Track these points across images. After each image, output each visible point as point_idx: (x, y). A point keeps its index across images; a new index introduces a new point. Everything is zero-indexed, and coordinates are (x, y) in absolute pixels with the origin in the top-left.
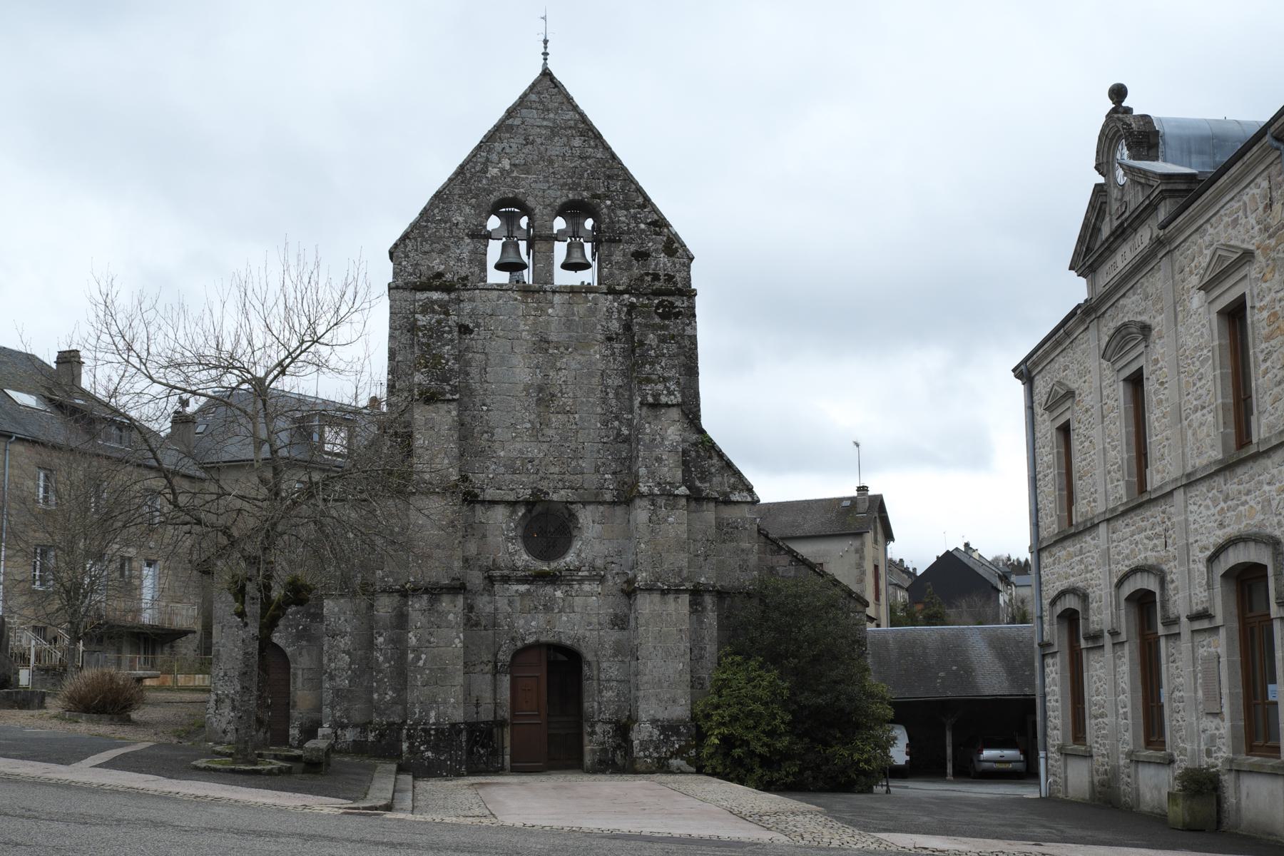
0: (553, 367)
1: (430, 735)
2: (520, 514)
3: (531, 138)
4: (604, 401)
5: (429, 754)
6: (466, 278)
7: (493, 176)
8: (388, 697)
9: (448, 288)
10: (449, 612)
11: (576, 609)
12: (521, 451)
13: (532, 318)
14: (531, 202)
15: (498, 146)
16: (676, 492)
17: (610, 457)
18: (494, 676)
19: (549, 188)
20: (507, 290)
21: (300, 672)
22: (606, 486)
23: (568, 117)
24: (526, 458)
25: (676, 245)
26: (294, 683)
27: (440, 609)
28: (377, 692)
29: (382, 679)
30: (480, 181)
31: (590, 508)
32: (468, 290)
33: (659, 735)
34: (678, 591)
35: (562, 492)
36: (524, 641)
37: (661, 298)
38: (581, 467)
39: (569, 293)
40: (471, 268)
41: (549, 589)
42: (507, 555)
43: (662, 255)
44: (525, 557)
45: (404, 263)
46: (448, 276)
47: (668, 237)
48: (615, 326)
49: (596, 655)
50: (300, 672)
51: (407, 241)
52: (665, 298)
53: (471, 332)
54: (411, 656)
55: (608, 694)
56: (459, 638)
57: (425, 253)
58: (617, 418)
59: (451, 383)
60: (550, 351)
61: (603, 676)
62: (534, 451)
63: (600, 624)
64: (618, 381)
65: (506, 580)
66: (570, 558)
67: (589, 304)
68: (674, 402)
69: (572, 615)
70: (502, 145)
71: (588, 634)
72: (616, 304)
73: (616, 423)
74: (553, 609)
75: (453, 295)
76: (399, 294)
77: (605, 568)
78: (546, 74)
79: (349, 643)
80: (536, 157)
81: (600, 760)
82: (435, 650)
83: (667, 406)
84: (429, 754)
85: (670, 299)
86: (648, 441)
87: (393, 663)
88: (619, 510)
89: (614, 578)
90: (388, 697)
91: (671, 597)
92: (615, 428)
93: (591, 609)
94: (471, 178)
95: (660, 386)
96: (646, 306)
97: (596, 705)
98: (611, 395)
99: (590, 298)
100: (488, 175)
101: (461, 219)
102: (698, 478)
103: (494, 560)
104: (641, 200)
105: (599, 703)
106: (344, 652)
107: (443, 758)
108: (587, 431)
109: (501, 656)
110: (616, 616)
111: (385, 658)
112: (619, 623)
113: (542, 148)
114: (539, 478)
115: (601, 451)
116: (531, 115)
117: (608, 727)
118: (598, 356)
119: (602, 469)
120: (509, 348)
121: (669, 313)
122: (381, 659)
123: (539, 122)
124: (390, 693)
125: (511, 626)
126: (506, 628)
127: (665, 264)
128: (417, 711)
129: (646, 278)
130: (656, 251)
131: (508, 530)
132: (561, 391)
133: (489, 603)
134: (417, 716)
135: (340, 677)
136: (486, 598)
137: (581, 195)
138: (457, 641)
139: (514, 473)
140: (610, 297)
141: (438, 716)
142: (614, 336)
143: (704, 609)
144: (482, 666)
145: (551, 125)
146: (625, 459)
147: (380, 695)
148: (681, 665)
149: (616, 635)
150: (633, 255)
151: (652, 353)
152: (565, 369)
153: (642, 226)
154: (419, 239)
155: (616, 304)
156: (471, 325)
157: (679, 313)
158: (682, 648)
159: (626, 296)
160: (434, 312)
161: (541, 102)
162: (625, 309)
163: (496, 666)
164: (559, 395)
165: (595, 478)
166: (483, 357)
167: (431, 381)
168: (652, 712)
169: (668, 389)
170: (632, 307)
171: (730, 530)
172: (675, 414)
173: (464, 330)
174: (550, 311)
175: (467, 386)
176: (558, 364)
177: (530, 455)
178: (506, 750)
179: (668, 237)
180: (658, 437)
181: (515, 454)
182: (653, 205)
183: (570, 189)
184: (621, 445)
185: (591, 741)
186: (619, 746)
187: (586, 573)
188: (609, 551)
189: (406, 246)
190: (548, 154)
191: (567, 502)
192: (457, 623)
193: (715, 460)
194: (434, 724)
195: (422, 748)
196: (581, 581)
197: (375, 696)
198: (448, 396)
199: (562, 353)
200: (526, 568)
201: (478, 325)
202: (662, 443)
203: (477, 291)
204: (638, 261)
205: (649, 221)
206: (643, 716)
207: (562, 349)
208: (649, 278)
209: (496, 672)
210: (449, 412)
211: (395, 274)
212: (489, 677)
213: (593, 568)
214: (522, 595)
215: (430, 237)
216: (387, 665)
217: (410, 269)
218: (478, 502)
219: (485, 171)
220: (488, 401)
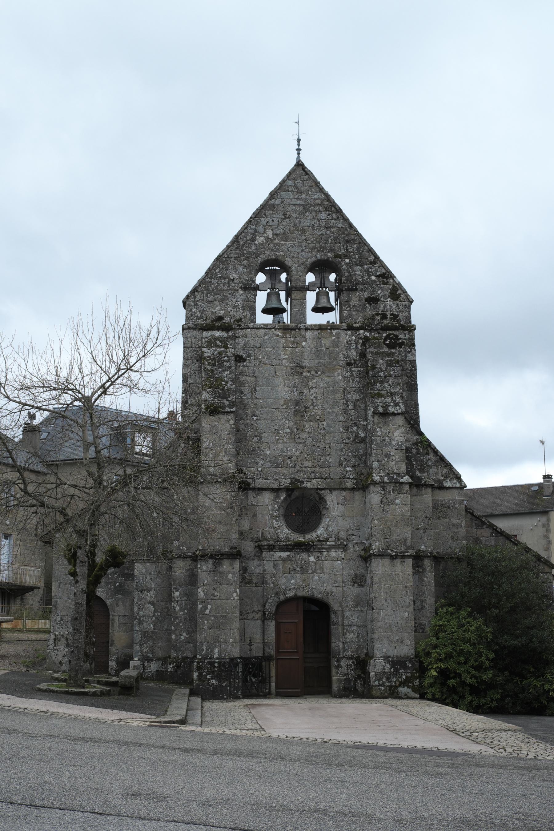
0: (306, 386)
1: (215, 667)
2: (282, 498)
3: (288, 213)
4: (346, 411)
5: (214, 681)
6: (240, 320)
7: (260, 243)
8: (182, 638)
9: (227, 328)
10: (229, 573)
11: (325, 570)
12: (282, 450)
13: (290, 349)
14: (288, 262)
15: (263, 220)
16: (402, 480)
17: (350, 454)
18: (263, 621)
19: (302, 251)
20: (271, 329)
21: (117, 618)
22: (347, 476)
23: (316, 197)
24: (286, 456)
25: (399, 292)
26: (113, 626)
27: (222, 570)
28: (174, 633)
29: (178, 624)
30: (250, 247)
31: (335, 493)
32: (242, 329)
33: (391, 669)
34: (403, 557)
35: (314, 481)
36: (285, 595)
37: (388, 333)
38: (328, 461)
39: (318, 330)
40: (244, 312)
41: (304, 555)
42: (273, 530)
43: (389, 299)
44: (286, 530)
45: (194, 310)
46: (227, 319)
47: (393, 286)
48: (353, 354)
49: (341, 606)
50: (117, 618)
51: (196, 293)
52: (391, 332)
53: (244, 360)
54: (200, 606)
55: (350, 636)
56: (236, 592)
57: (210, 302)
58: (355, 424)
59: (229, 399)
60: (304, 374)
61: (346, 622)
62: (293, 450)
63: (343, 582)
64: (356, 396)
65: (271, 548)
66: (320, 531)
67: (333, 338)
68: (399, 411)
69: (322, 575)
70: (267, 220)
71: (334, 589)
72: (354, 338)
73: (355, 428)
74: (307, 571)
75: (231, 333)
76: (190, 333)
77: (347, 539)
78: (300, 165)
79: (154, 596)
80: (292, 228)
81: (344, 688)
82: (219, 602)
83: (394, 414)
84: (214, 681)
85: (396, 333)
86: (379, 442)
87: (186, 611)
88: (358, 495)
89: (354, 546)
90: (182, 638)
91: (398, 561)
92: (353, 432)
93: (337, 571)
94: (243, 245)
95: (388, 400)
96: (376, 338)
97: (341, 644)
98: (351, 407)
99: (334, 334)
100: (257, 243)
101: (236, 276)
102: (418, 469)
103: (262, 533)
104: (372, 258)
105: (344, 643)
106: (150, 603)
107: (224, 685)
108: (332, 435)
109: (268, 606)
110: (356, 576)
111: (181, 608)
112: (358, 581)
113: (297, 221)
114: (296, 471)
115: (344, 450)
116: (289, 197)
117: (350, 662)
118: (340, 378)
119: (344, 463)
120: (273, 372)
121: (395, 343)
122: (177, 608)
123: (294, 201)
124: (184, 634)
125: (276, 584)
126: (272, 585)
127: (391, 306)
128: (204, 648)
129: (377, 317)
130: (384, 296)
131: (273, 510)
132: (312, 404)
133: (259, 566)
134: (204, 652)
135: (147, 622)
136: (256, 562)
137: (327, 255)
138: (235, 595)
139: (277, 467)
140: (349, 332)
141: (220, 653)
142: (353, 362)
143: (424, 570)
144: (254, 614)
145: (303, 203)
146: (361, 455)
147: (176, 636)
148: (407, 614)
149: (353, 591)
150: (366, 300)
151: (382, 374)
152: (315, 387)
153: (373, 278)
154: (205, 292)
155: (354, 338)
156: (244, 356)
157: (402, 343)
158: (407, 600)
159: (362, 331)
160: (216, 346)
161: (296, 186)
162: (361, 341)
163: (264, 614)
164: (311, 407)
165: (339, 470)
166: (253, 379)
167: (214, 398)
168: (384, 650)
169: (394, 401)
170: (366, 339)
171: (443, 509)
172: (400, 420)
173: (239, 359)
174: (304, 344)
175: (241, 402)
176: (310, 384)
177: (289, 453)
178: (272, 679)
179: (393, 286)
180: (387, 438)
181: (278, 452)
182: (381, 261)
183: (318, 251)
184: (359, 445)
185: (337, 673)
186: (359, 677)
187: (333, 543)
188: (350, 526)
189: (195, 297)
190: (301, 225)
191: (318, 489)
192: (234, 581)
193: (431, 456)
194: (217, 658)
195: (208, 677)
196: (329, 549)
197: (173, 637)
198: (228, 409)
199: (313, 375)
200: (287, 539)
201: (249, 356)
202: (390, 443)
203: (249, 330)
204: (370, 304)
205: (378, 274)
206: (378, 654)
207: (313, 373)
208: (379, 317)
209: (264, 619)
210: (228, 421)
211: (187, 318)
212: (259, 623)
213: (338, 539)
214: (284, 560)
215: (213, 290)
216: (182, 613)
217: (198, 314)
218: (250, 489)
219: (254, 239)
220: (257, 413)
